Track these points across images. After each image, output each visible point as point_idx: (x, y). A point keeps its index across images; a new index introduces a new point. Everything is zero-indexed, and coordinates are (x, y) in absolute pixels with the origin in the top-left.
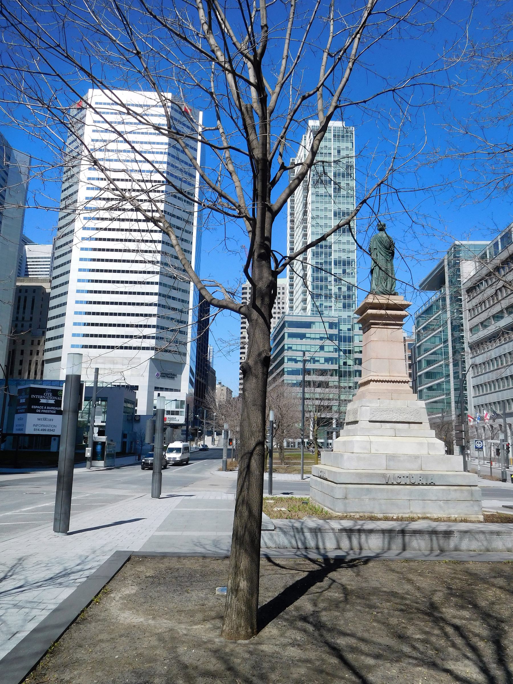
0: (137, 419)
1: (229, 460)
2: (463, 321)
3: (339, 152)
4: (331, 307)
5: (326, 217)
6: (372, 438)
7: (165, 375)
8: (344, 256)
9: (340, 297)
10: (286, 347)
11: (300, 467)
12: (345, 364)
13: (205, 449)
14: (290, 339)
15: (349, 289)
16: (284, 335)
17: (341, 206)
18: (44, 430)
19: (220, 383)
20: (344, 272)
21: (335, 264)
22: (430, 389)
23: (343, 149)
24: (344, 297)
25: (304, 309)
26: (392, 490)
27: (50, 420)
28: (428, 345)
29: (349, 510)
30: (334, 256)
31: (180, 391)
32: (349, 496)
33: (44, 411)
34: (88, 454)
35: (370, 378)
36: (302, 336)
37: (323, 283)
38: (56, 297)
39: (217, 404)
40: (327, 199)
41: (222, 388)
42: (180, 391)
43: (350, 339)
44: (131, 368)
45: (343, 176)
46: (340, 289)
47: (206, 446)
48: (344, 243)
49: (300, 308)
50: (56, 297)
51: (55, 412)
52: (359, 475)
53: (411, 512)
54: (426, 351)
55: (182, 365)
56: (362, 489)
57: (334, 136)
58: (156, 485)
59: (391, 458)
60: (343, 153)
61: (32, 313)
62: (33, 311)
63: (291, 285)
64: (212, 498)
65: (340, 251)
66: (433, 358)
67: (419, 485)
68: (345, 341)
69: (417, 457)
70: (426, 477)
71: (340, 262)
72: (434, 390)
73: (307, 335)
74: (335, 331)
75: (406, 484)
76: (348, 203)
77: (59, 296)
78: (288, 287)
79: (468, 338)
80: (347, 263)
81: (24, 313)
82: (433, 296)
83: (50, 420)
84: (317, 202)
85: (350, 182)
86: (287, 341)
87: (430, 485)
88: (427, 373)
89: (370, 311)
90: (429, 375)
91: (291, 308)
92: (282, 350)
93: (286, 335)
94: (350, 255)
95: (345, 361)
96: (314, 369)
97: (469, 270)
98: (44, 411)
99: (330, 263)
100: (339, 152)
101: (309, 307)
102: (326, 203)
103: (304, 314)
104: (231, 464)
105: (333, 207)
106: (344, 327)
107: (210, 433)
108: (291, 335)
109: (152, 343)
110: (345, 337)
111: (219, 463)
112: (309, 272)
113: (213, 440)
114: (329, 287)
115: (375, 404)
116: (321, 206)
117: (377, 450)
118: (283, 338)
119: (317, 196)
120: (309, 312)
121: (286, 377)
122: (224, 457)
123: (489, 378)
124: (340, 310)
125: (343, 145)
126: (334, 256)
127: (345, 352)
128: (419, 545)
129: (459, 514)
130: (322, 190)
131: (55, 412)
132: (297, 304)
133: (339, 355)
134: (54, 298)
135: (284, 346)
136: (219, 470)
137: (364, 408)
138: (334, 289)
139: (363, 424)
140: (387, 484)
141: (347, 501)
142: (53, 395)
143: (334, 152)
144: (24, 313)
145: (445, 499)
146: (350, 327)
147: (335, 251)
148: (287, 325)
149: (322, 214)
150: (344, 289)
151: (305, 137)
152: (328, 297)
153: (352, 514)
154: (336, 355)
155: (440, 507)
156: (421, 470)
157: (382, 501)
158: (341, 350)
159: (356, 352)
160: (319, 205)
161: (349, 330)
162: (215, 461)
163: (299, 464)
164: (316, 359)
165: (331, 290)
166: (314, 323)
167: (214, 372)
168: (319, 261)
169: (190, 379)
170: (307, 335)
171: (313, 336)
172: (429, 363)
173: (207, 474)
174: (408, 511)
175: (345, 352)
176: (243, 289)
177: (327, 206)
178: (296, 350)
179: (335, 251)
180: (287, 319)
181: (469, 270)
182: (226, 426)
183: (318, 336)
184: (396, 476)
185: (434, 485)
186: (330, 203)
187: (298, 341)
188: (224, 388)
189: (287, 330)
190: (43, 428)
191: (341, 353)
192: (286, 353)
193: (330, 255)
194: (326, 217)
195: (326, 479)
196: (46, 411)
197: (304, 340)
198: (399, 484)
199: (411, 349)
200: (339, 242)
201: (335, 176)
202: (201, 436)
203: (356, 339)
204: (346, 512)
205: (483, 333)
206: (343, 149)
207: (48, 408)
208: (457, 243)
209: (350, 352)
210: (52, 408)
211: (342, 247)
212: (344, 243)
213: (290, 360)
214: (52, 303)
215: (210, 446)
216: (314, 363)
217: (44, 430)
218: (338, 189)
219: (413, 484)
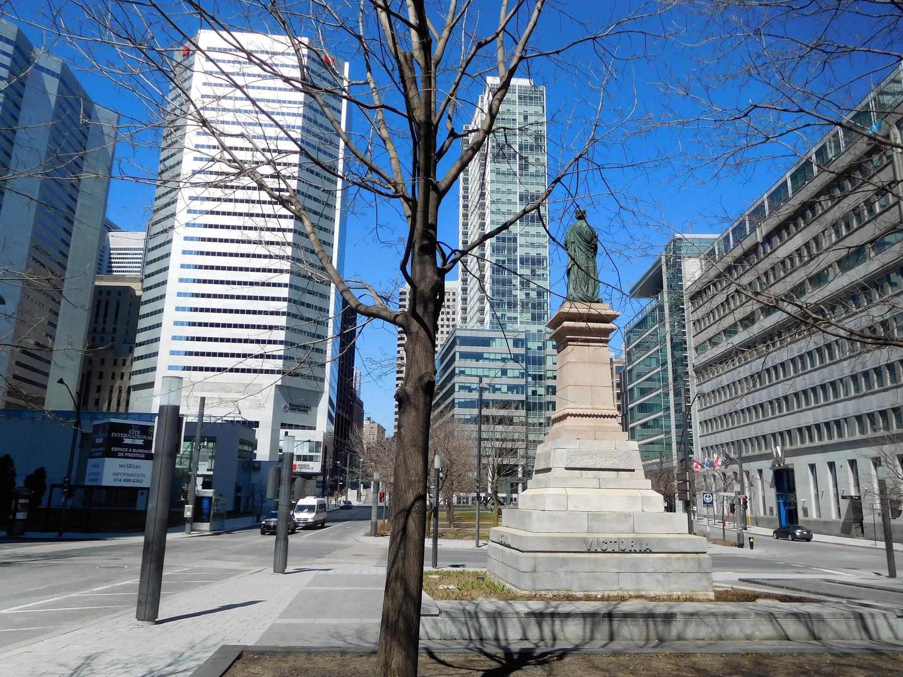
0: (257, 466)
1: (380, 522)
2: (687, 337)
3: (526, 118)
4: (516, 318)
5: (509, 202)
6: (570, 491)
7: (294, 407)
8: (533, 252)
9: (527, 304)
10: (457, 371)
11: (474, 530)
12: (534, 393)
13: (348, 506)
14: (463, 360)
15: (539, 294)
16: (454, 355)
17: (529, 187)
18: (129, 481)
19: (369, 419)
20: (533, 271)
21: (522, 263)
22: (645, 425)
23: (531, 115)
24: (534, 307)
25: (482, 322)
26: (596, 561)
27: (137, 467)
28: (642, 368)
29: (539, 587)
30: (520, 252)
31: (314, 429)
32: (539, 569)
33: (129, 455)
34: (188, 514)
35: (566, 412)
36: (478, 357)
37: (507, 288)
38: (149, 301)
39: (365, 446)
40: (510, 178)
41: (372, 425)
42: (314, 429)
43: (541, 361)
44: (253, 400)
45: (532, 150)
46: (527, 295)
47: (350, 503)
48: (533, 236)
49: (475, 319)
50: (149, 301)
51: (143, 456)
52: (553, 540)
53: (621, 589)
54: (639, 376)
55: (318, 394)
56: (557, 558)
57: (520, 98)
58: (281, 555)
59: (594, 516)
60: (531, 119)
61: (116, 323)
62: (118, 321)
63: (464, 290)
64: (355, 572)
65: (527, 246)
66: (648, 385)
67: (630, 552)
68: (534, 364)
69: (627, 516)
70: (640, 541)
71: (527, 260)
72: (649, 427)
73: (485, 356)
74: (521, 351)
75: (613, 552)
76: (538, 184)
77: (154, 300)
78: (460, 292)
79: (693, 359)
80: (537, 261)
81: (105, 322)
82: (647, 304)
83: (137, 467)
84: (498, 182)
85: (540, 157)
86: (459, 363)
87: (645, 552)
88: (640, 405)
89: (566, 324)
90: (643, 408)
91: (464, 319)
92: (452, 374)
93: (457, 355)
94: (540, 251)
95: (534, 389)
96: (493, 400)
97: (692, 270)
98: (129, 455)
99: (515, 262)
100: (526, 118)
101: (488, 318)
102: (510, 183)
103: (481, 328)
104: (382, 526)
105: (519, 189)
106: (533, 345)
107: (355, 486)
108: (464, 356)
109: (278, 364)
110: (534, 358)
111: (366, 526)
112: (488, 273)
113: (359, 495)
114: (514, 293)
115: (574, 446)
116: (504, 188)
117: (575, 507)
118: (453, 359)
119: (498, 173)
120: (487, 326)
121: (457, 410)
122: (374, 518)
123: (754, 400)
124: (528, 323)
125: (531, 109)
126: (520, 252)
127: (534, 377)
128: (631, 633)
129: (683, 590)
130: (504, 167)
131: (143, 456)
132: (471, 314)
133: (527, 382)
134: (146, 302)
135: (454, 369)
136: (367, 535)
137: (558, 451)
138: (520, 295)
139: (558, 472)
140: (589, 552)
141: (536, 575)
142: (142, 434)
143: (519, 119)
144: (105, 322)
145: (664, 570)
146: (540, 344)
147: (521, 246)
148: (458, 341)
149: (504, 198)
150: (533, 294)
151: (482, 98)
152: (512, 305)
153: (543, 593)
154: (522, 382)
155: (658, 581)
156: (634, 532)
157: (583, 575)
158: (530, 375)
159: (549, 378)
160: (499, 186)
161: (539, 348)
162: (360, 522)
163: (474, 526)
164: (497, 386)
165: (516, 296)
166: (493, 339)
167: (361, 404)
168: (501, 258)
169: (329, 413)
170: (485, 356)
171: (492, 356)
172: (643, 392)
173: (350, 541)
174: (617, 587)
175: (534, 377)
176: (401, 294)
177: (510, 186)
178: (471, 376)
179: (521, 246)
180: (458, 333)
181: (692, 270)
182: (376, 476)
183: (499, 357)
184: (601, 540)
185: (651, 552)
186: (515, 183)
187: (473, 363)
188: (375, 426)
189: (458, 348)
190: (126, 477)
191: (530, 379)
192: (457, 379)
193: (515, 250)
194: (509, 202)
195: (509, 546)
196: (131, 455)
197: (481, 361)
198: (604, 552)
199: (620, 375)
200: (527, 234)
201: (521, 148)
202: (342, 490)
203: (549, 361)
204: (535, 590)
205: (712, 353)
206: (531, 115)
207: (134, 450)
208: (678, 236)
209: (541, 377)
210: (140, 451)
211: (530, 240)
212: (533, 236)
213: (461, 388)
214: (144, 310)
215: (355, 503)
216: (494, 392)
217: (129, 481)
218: (524, 167)
219: (623, 552)
